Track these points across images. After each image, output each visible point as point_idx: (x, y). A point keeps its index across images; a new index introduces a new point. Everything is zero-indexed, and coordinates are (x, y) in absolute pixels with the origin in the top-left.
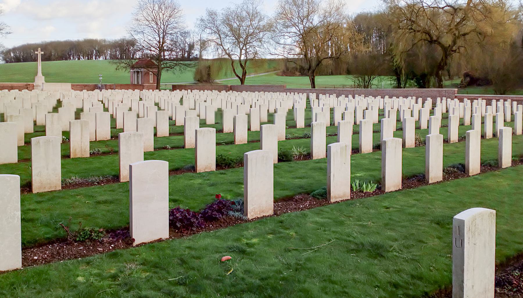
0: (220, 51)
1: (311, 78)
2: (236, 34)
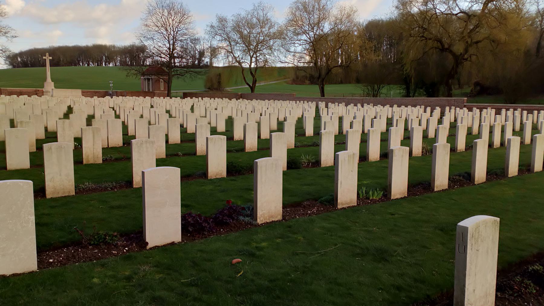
0: (230, 59)
1: (320, 87)
2: (246, 40)
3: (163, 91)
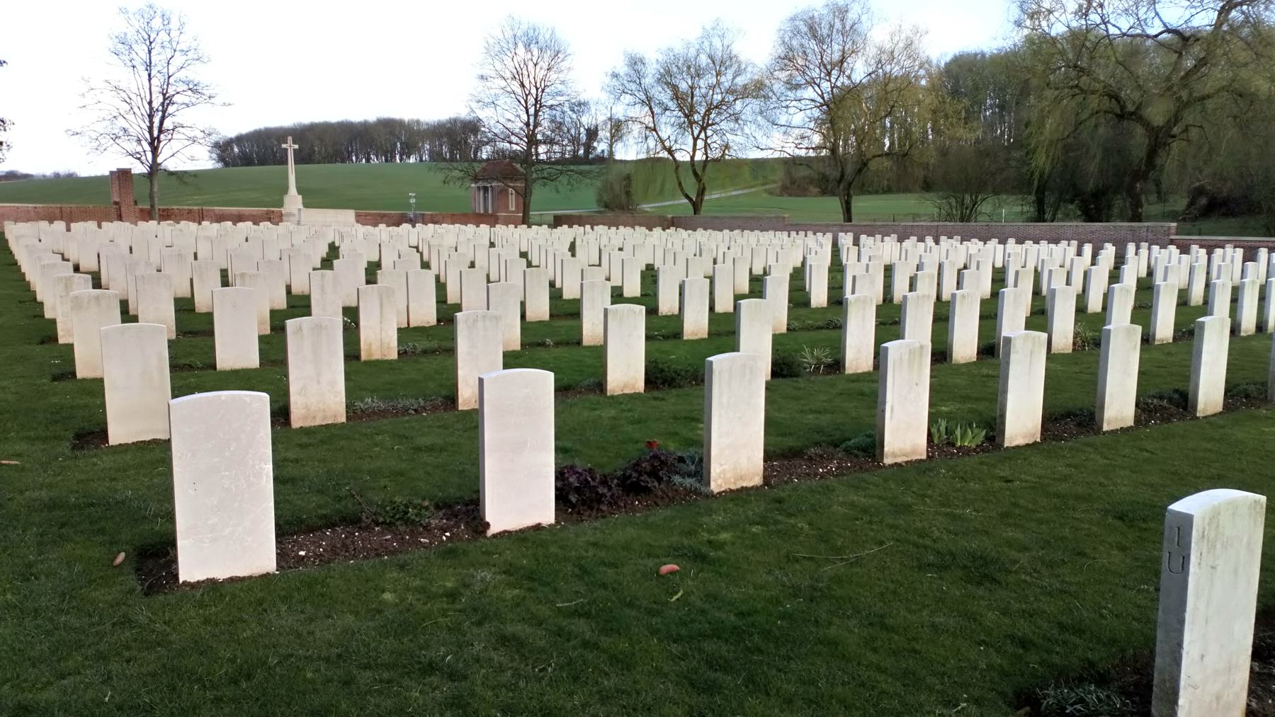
0: (651, 143)
1: (843, 201)
2: (685, 102)
3: (513, 212)
